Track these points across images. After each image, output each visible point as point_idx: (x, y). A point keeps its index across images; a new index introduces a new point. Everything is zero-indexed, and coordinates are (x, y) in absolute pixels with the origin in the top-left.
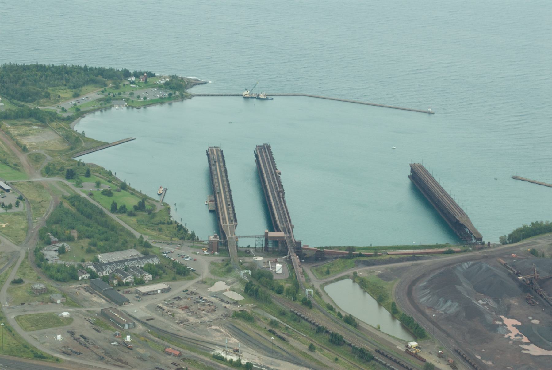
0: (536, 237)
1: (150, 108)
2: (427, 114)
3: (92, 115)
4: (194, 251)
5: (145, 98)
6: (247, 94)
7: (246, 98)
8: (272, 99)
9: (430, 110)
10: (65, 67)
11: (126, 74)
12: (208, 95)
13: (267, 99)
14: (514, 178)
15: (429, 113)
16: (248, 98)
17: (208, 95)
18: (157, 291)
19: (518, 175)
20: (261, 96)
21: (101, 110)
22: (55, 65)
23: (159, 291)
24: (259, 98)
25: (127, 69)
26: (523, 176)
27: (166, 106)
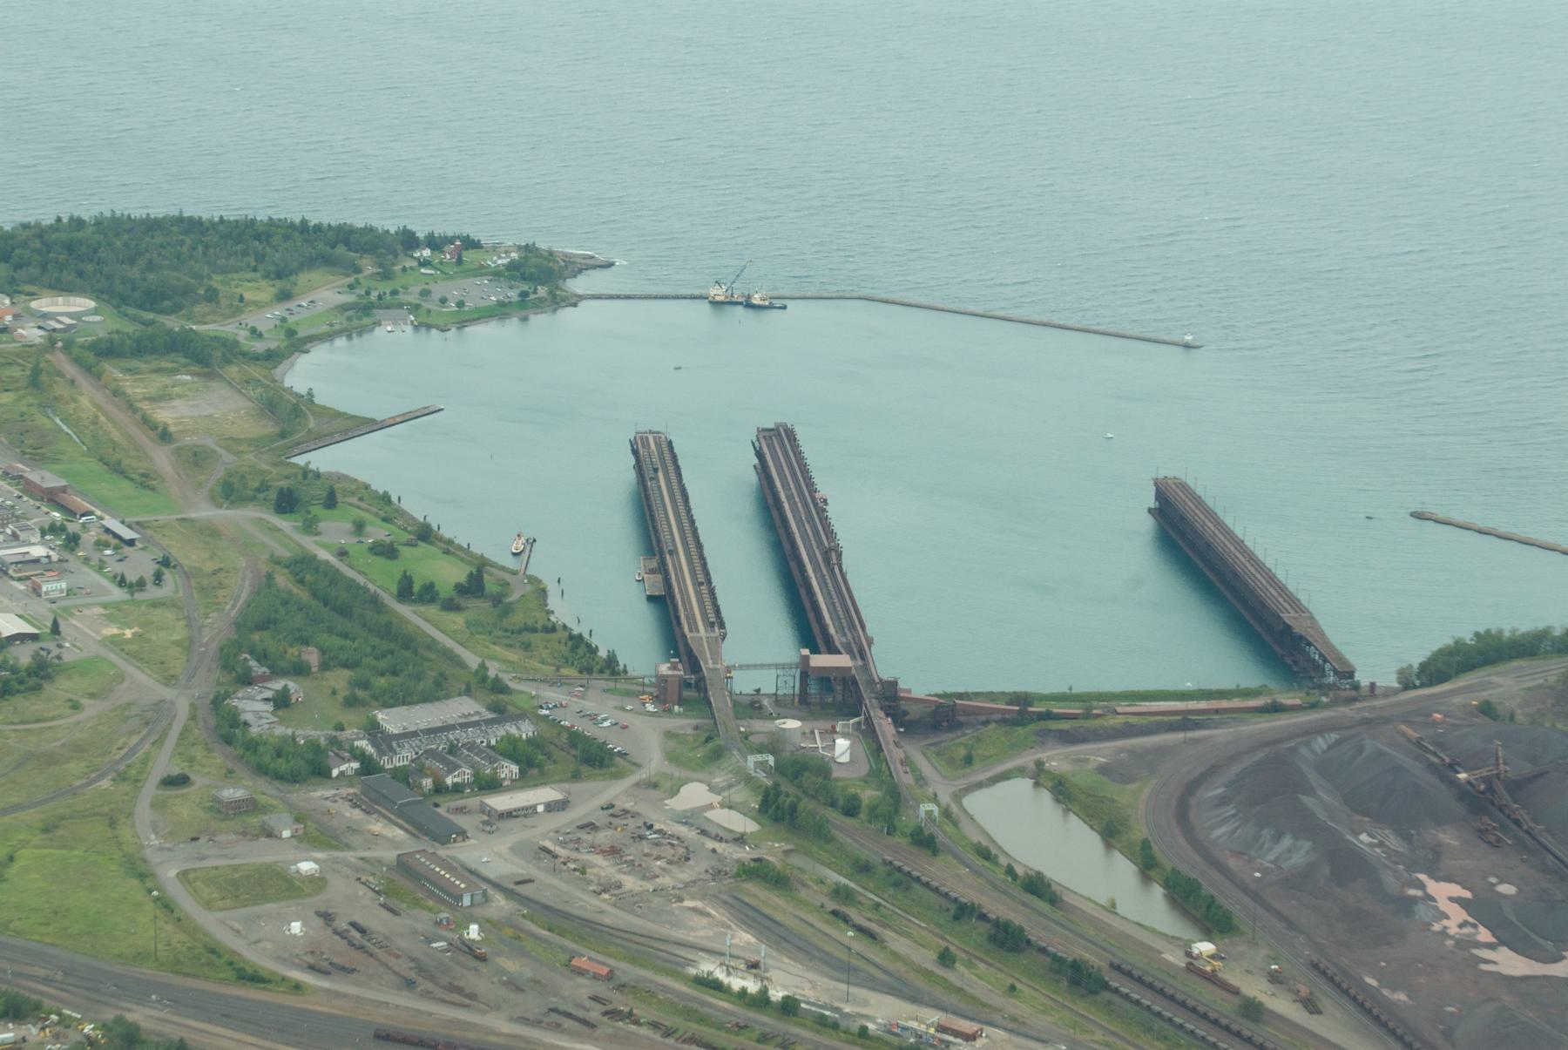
2: (1180, 350)
6: (718, 293)
7: (716, 304)
8: (784, 307)
9: (1188, 338)
13: (771, 307)
14: (1418, 516)
15: (1187, 346)
16: (722, 303)
18: (534, 807)
20: (756, 300)
23: (540, 809)
24: (750, 306)
27: (513, 324)
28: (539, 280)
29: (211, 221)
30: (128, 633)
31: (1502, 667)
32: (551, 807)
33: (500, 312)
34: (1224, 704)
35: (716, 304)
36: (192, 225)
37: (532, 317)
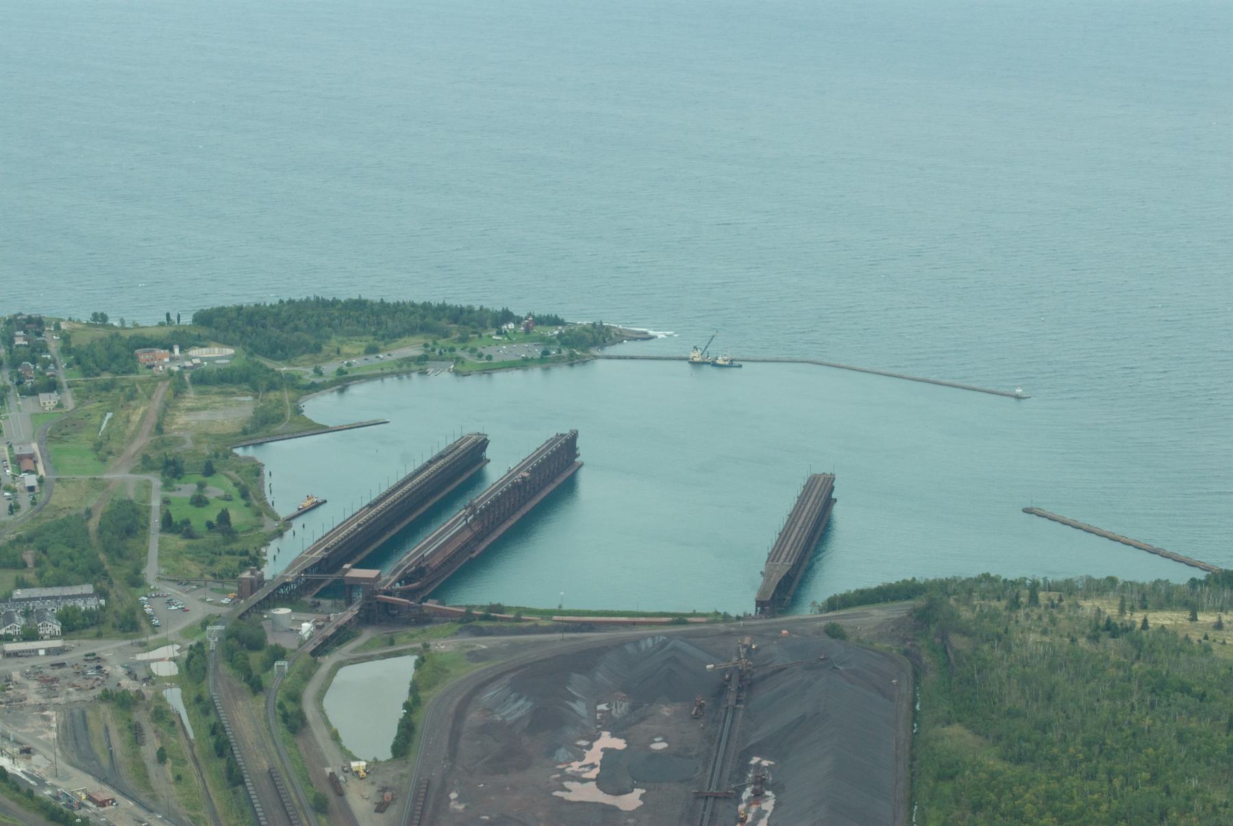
0: (872, 606)
1: (498, 376)
2: (1013, 400)
3: (378, 382)
4: (202, 596)
5: (489, 358)
6: (696, 356)
7: (694, 363)
8: (740, 366)
9: (1019, 391)
10: (470, 310)
11: (507, 316)
12: (625, 358)
13: (731, 366)
14: (1027, 511)
15: (1018, 397)
16: (697, 363)
17: (625, 358)
18: (36, 651)
19: (1034, 506)
20: (720, 362)
21: (398, 375)
22: (386, 301)
23: (42, 652)
24: (714, 364)
25: (511, 310)
26: (1047, 509)
27: (536, 373)
28: (580, 344)
29: (301, 301)
30: (765, 763)
31: (877, 605)
32: (49, 652)
33: (524, 364)
34: (613, 619)
35: (694, 363)
36: (322, 304)
37: (86, 317)
